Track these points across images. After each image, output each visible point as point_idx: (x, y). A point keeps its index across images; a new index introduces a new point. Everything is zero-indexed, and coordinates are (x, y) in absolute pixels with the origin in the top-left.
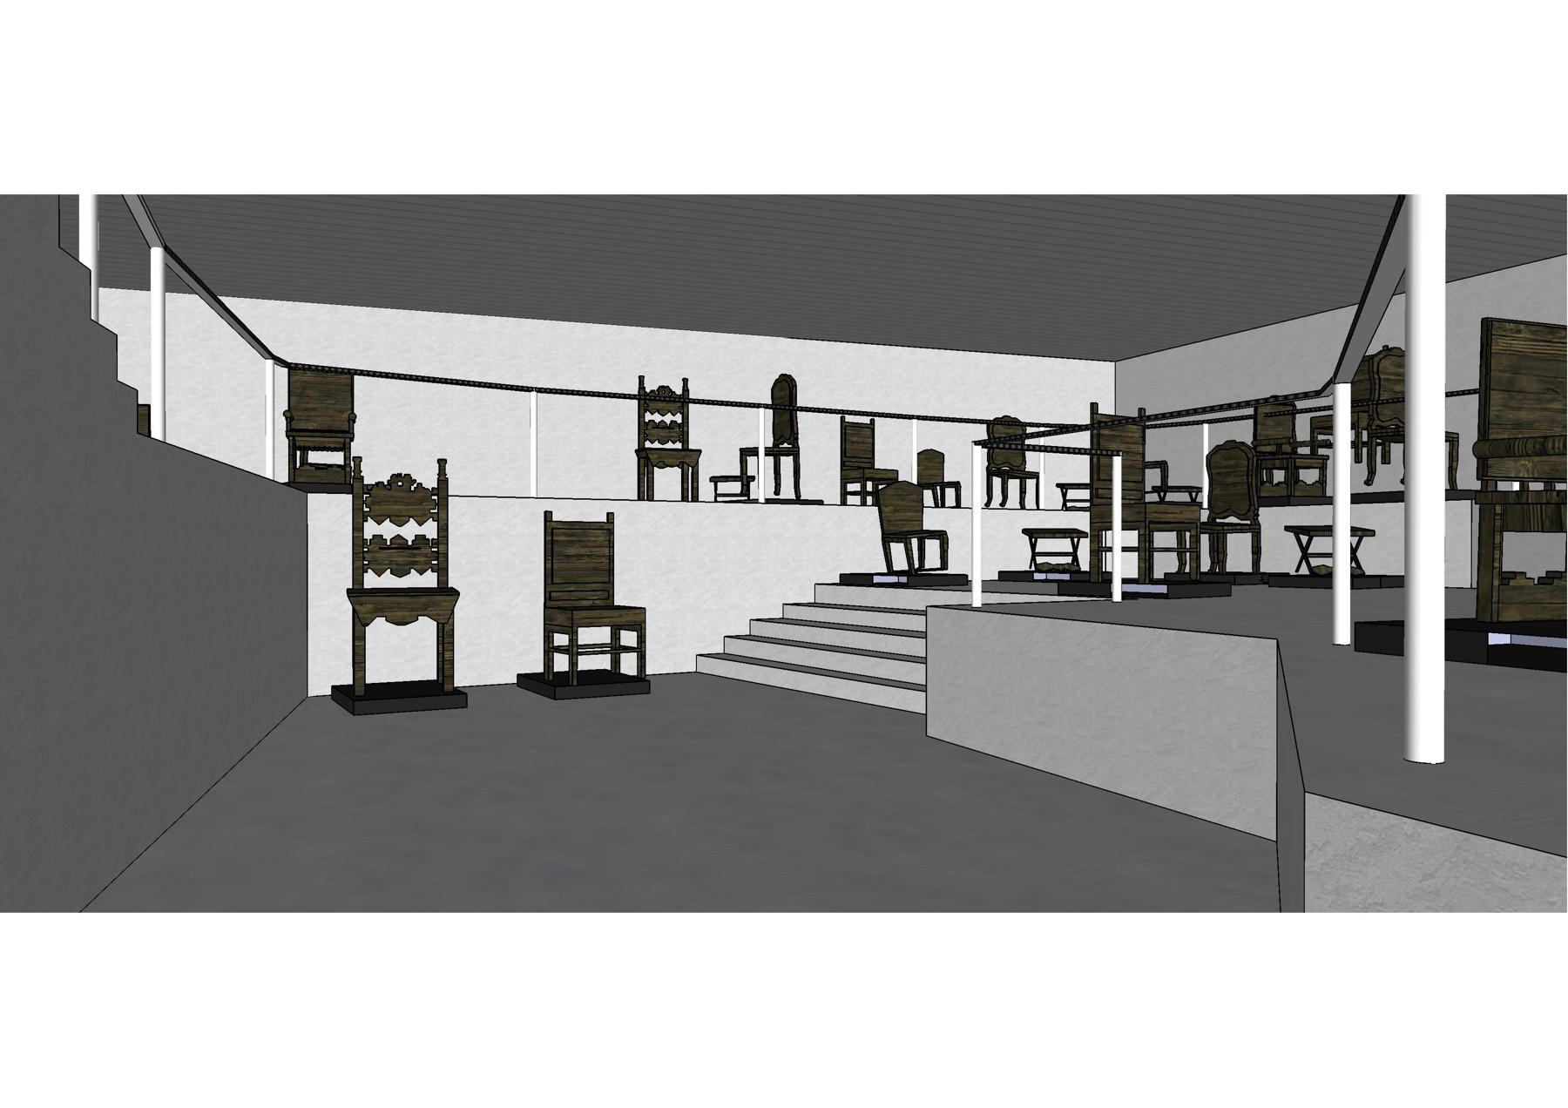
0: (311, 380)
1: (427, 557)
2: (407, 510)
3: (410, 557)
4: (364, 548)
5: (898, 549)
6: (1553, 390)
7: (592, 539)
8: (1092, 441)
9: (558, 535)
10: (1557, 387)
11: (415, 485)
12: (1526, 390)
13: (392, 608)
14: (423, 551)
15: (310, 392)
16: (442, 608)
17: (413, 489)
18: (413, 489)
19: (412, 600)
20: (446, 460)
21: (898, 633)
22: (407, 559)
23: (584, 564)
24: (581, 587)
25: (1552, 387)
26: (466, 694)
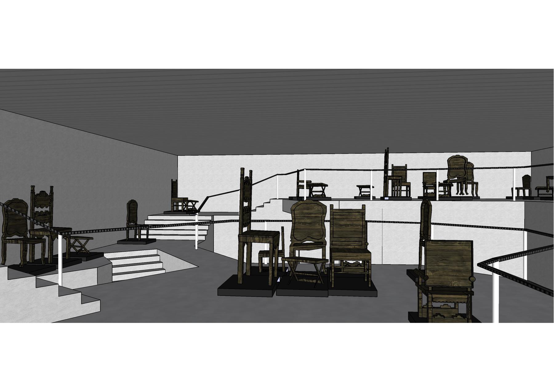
0: (428, 174)
7: (353, 217)
8: (448, 166)
9: (335, 215)
15: (427, 177)
20: (34, 186)
21: (151, 270)
23: (349, 228)
24: (348, 240)
26: (272, 297)
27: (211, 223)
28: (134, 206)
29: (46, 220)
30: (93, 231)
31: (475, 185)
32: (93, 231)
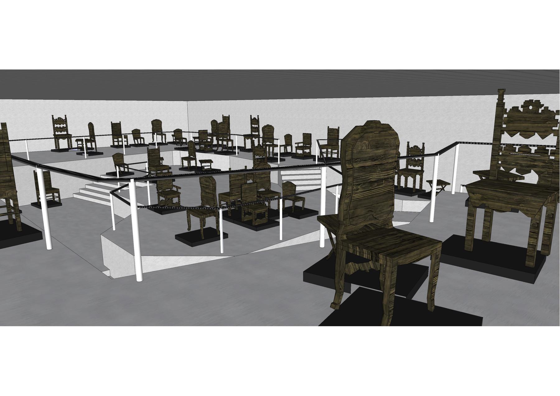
1: (545, 163)
2: (533, 127)
3: (531, 161)
4: (499, 155)
5: (136, 141)
6: (371, 211)
10: (372, 209)
11: (543, 108)
12: (360, 215)
13: (493, 199)
14: (419, 162)
16: (531, 206)
17: (540, 111)
18: (540, 111)
19: (508, 196)
22: (529, 163)
25: (370, 210)
27: (261, 162)
28: (191, 145)
29: (417, 164)
30: (165, 132)
31: (268, 147)
32: (165, 132)
